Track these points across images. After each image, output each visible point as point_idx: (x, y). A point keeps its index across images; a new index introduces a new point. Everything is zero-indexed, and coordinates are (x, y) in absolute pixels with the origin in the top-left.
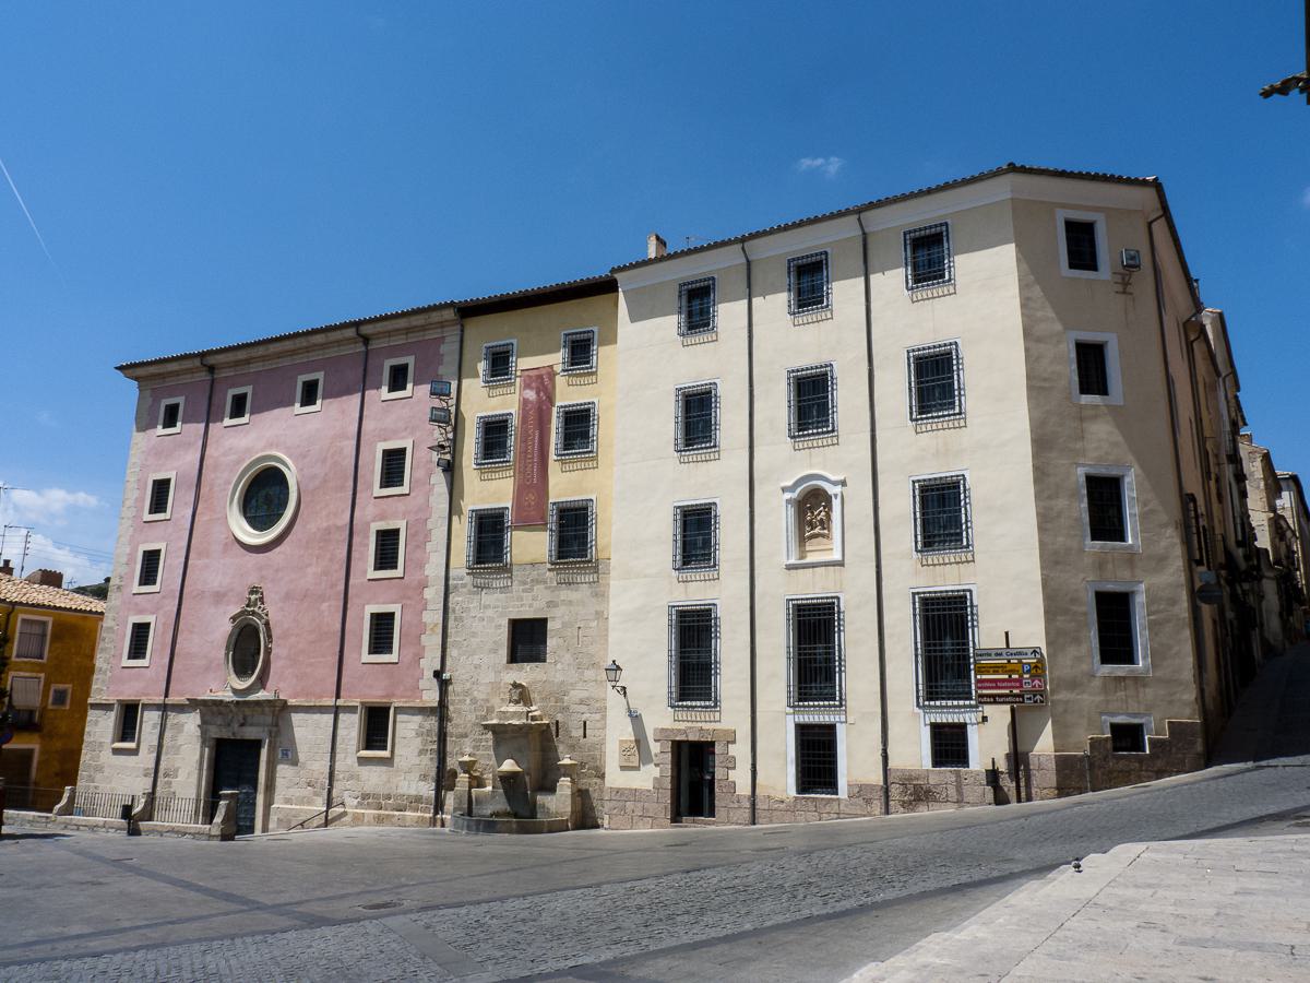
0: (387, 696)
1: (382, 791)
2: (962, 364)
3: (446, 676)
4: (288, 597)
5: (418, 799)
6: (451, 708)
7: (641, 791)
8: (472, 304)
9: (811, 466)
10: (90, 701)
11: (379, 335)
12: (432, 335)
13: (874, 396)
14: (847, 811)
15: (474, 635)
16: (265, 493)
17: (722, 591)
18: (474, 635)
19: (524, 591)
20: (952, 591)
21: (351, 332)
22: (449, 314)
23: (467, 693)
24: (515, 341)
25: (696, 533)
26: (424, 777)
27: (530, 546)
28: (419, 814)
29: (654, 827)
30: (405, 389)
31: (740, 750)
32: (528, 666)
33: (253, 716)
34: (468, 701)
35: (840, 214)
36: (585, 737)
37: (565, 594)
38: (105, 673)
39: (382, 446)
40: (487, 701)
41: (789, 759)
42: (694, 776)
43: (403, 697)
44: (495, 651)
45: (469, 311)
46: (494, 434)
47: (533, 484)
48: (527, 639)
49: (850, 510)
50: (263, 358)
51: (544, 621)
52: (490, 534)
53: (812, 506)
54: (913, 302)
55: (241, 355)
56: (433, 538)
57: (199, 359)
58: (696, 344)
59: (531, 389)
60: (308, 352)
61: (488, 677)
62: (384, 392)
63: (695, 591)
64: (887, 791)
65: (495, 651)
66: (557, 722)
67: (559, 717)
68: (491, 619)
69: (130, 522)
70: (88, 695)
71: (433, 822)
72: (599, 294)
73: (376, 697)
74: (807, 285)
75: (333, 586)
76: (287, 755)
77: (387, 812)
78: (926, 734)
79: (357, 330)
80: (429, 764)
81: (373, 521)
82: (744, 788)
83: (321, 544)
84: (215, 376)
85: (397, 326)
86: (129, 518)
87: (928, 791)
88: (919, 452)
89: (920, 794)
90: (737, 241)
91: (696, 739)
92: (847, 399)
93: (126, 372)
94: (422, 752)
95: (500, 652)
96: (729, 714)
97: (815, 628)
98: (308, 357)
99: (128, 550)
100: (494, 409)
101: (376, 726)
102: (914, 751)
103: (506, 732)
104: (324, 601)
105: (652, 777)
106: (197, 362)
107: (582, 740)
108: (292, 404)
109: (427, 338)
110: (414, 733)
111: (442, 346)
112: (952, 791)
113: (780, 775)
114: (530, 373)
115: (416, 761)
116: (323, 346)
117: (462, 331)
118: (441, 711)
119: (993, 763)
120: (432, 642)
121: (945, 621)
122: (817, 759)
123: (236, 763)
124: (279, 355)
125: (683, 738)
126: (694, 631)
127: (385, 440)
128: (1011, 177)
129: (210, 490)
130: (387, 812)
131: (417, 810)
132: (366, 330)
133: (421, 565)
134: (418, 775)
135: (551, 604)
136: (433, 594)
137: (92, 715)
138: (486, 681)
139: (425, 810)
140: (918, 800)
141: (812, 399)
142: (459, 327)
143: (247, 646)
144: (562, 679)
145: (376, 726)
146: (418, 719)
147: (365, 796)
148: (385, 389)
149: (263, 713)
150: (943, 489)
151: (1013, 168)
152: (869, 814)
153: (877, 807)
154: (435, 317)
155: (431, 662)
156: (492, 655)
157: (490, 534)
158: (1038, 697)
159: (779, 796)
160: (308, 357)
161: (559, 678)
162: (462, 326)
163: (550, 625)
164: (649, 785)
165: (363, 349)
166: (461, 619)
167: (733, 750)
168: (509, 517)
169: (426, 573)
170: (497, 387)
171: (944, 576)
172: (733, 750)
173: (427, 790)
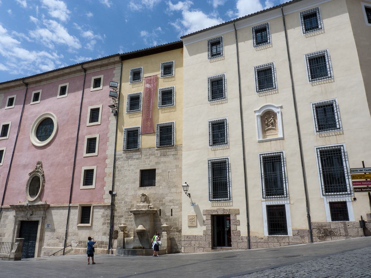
0: (90, 202)
3: (114, 193)
5: (102, 243)
7: (198, 236)
9: (266, 102)
13: (292, 74)
14: (293, 241)
15: (126, 176)
17: (231, 153)
18: (126, 176)
21: (79, 68)
22: (117, 59)
23: (123, 199)
25: (218, 133)
27: (149, 141)
28: (102, 249)
29: (205, 250)
31: (242, 217)
34: (123, 203)
36: (172, 215)
37: (163, 159)
40: (131, 202)
42: (221, 229)
43: (96, 202)
44: (134, 182)
45: (125, 57)
46: (134, 101)
47: (148, 119)
48: (148, 177)
52: (132, 139)
53: (268, 119)
57: (81, 66)
61: (131, 193)
62: (92, 89)
63: (219, 153)
64: (311, 231)
65: (134, 182)
66: (160, 210)
67: (161, 208)
68: (133, 170)
71: (108, 252)
73: (85, 202)
76: (49, 227)
80: (107, 229)
82: (244, 232)
88: (313, 93)
89: (327, 233)
91: (222, 214)
94: (104, 224)
95: (136, 183)
96: (236, 202)
97: (272, 165)
101: (85, 214)
102: (322, 214)
105: (202, 230)
107: (171, 217)
110: (101, 216)
112: (342, 231)
113: (260, 226)
114: (148, 78)
115: (102, 227)
117: (122, 65)
118: (112, 207)
120: (109, 180)
121: (331, 159)
122: (277, 220)
125: (216, 213)
126: (219, 173)
127: (92, 105)
131: (101, 247)
133: (105, 151)
136: (110, 162)
138: (130, 193)
139: (104, 247)
141: (265, 78)
153: (307, 239)
155: (108, 188)
157: (132, 139)
159: (260, 236)
161: (161, 192)
163: (157, 171)
164: (201, 234)
166: (121, 170)
167: (238, 218)
168: (140, 131)
169: (107, 154)
171: (330, 140)
172: (238, 218)
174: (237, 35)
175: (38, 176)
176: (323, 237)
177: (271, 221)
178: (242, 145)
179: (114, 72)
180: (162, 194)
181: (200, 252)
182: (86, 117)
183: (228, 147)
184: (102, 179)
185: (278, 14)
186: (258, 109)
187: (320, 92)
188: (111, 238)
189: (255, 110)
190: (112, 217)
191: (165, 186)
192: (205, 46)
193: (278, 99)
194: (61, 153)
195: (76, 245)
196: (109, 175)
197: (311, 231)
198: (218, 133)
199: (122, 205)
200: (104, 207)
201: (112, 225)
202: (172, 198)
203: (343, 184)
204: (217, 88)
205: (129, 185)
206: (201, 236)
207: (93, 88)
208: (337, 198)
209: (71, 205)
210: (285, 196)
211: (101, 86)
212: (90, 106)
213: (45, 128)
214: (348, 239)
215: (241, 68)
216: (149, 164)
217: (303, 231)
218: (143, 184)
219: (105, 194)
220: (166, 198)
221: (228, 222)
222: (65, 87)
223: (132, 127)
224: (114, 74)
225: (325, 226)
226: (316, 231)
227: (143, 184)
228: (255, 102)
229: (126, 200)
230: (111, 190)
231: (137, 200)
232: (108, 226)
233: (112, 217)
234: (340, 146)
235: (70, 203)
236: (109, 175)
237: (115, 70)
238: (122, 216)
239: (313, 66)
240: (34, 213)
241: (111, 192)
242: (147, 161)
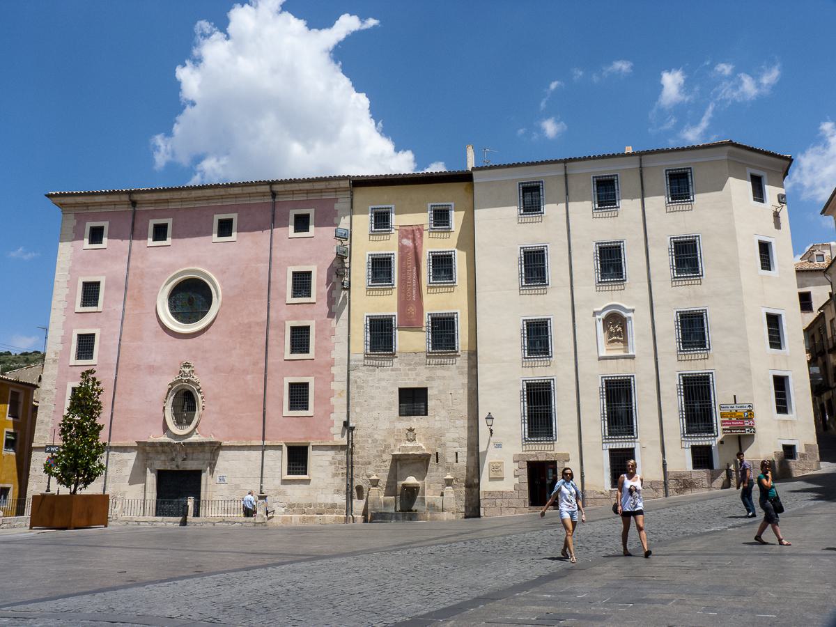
0: (305, 439)
1: (303, 501)
2: (669, 252)
4: (217, 370)
5: (334, 506)
6: (357, 446)
7: (507, 492)
8: (445, 174)
9: (612, 300)
10: (33, 445)
11: (285, 193)
12: (326, 196)
13: (649, 263)
15: (372, 398)
16: (191, 297)
17: (555, 370)
18: (372, 398)
19: (409, 370)
20: (702, 373)
22: (346, 184)
23: (369, 436)
24: (393, 206)
25: (537, 337)
26: (338, 491)
27: (413, 341)
28: (335, 515)
29: (522, 510)
30: (231, 235)
32: (414, 418)
33: (193, 453)
34: (370, 441)
35: (556, 162)
36: (457, 462)
37: (440, 372)
38: (47, 424)
39: (291, 269)
40: (385, 440)
41: (605, 468)
42: (542, 481)
43: (317, 439)
44: (390, 409)
48: (413, 400)
49: (637, 326)
50: (182, 200)
51: (426, 389)
54: (518, 223)
55: (307, 186)
56: (337, 333)
57: (128, 196)
58: (533, 222)
59: (408, 238)
60: (236, 197)
61: (384, 425)
62: (150, 242)
63: (538, 372)
64: (665, 484)
65: (390, 409)
66: (437, 453)
67: (439, 450)
69: (62, 313)
70: (32, 440)
71: (346, 520)
72: (423, 184)
73: (298, 439)
74: (606, 194)
75: (255, 364)
77: (309, 516)
78: (606, 455)
79: (130, 197)
80: (341, 483)
81: (287, 320)
83: (243, 334)
84: (276, 200)
85: (301, 188)
86: (61, 309)
87: (692, 482)
89: (685, 484)
90: (560, 161)
91: (544, 460)
92: (555, 267)
93: (53, 199)
94: (335, 475)
95: (393, 409)
96: (563, 446)
97: (618, 396)
98: (222, 202)
99: (62, 333)
100: (380, 250)
101: (298, 458)
102: (681, 461)
103: (408, 459)
104: (248, 374)
106: (266, 188)
108: (210, 234)
109: (197, 206)
110: (328, 463)
111: (336, 205)
113: (598, 476)
114: (406, 228)
115: (331, 480)
116: (236, 196)
117: (352, 195)
118: (349, 449)
119: (58, 491)
120: (339, 403)
121: (697, 392)
123: (178, 486)
124: (196, 199)
126: (539, 401)
127: (294, 265)
128: (730, 148)
129: (139, 292)
130: (309, 516)
131: (332, 513)
132: (276, 188)
133: (328, 352)
134: (332, 490)
135: (429, 379)
136: (339, 371)
137: (34, 453)
138: (382, 427)
139: (341, 513)
140: (686, 487)
141: (611, 261)
142: (349, 192)
143: (185, 401)
144: (439, 426)
145: (298, 458)
146: (331, 453)
147: (291, 506)
148: (86, 240)
149: (203, 451)
150: (692, 317)
151: (731, 143)
152: (657, 497)
153: (661, 493)
154: (334, 184)
155: (339, 417)
156: (387, 411)
157: (381, 334)
158: (752, 430)
159: (600, 490)
160: (293, 198)
161: (438, 425)
162: (352, 192)
165: (272, 200)
168: (396, 323)
169: (332, 356)
170: (381, 235)
171: (696, 365)
173: (341, 499)
174: (568, 183)
175: (190, 389)
176: (681, 489)
177: (615, 470)
178: (573, 362)
179: (337, 206)
180: (441, 427)
181: (510, 514)
182: (286, 286)
183: (548, 364)
184: (324, 399)
185: (558, 170)
186: (600, 309)
187: (536, 305)
188: (350, 498)
189: (595, 310)
190: (350, 465)
191: (444, 417)
192: (515, 192)
193: (628, 297)
194: (235, 348)
195: (283, 510)
196: (340, 394)
197: (665, 484)
198: (537, 337)
199: (367, 445)
200: (333, 448)
201: (350, 477)
202: (457, 435)
203: (630, 426)
204: (534, 266)
205: (379, 412)
206: (513, 492)
207: (152, 239)
208: (702, 441)
209: (267, 443)
210: (686, 435)
211: (233, 234)
212: (290, 266)
213: (191, 297)
214: (711, 492)
215: (572, 241)
216: (414, 379)
217: (657, 482)
218: (404, 412)
219: (333, 426)
220: (447, 435)
221: (550, 471)
222: (101, 229)
223: (379, 314)
224: (337, 210)
225: (684, 476)
226: (673, 483)
227: (404, 412)
228: (599, 299)
229: (376, 436)
230: (346, 419)
231: (396, 437)
232: (343, 480)
233: (350, 465)
234: (709, 373)
235: (263, 440)
236: (340, 394)
237: (337, 202)
238: (370, 463)
239: (528, 266)
240: (190, 457)
241: (346, 424)
242: (412, 374)
